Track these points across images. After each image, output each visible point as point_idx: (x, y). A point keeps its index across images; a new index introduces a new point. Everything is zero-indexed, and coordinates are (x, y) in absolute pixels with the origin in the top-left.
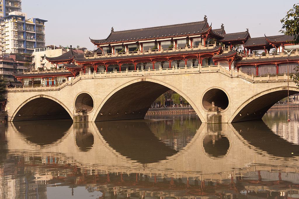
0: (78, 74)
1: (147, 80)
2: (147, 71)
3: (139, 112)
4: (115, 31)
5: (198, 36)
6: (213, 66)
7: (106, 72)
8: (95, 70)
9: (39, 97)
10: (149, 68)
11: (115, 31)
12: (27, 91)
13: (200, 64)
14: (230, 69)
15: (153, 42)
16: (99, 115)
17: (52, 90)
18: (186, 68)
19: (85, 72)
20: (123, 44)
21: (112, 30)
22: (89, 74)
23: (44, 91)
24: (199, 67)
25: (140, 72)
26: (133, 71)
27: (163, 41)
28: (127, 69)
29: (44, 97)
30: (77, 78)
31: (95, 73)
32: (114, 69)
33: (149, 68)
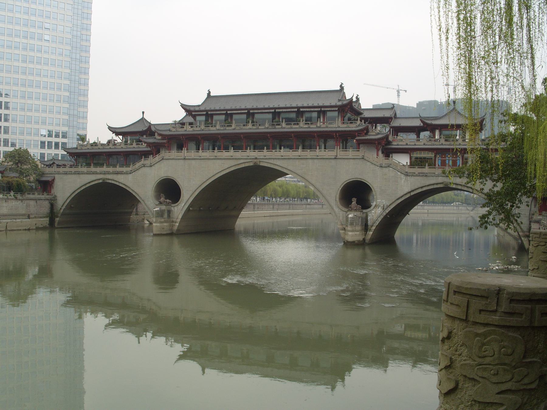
0: (158, 152)
1: (262, 164)
2: (263, 151)
3: (201, 209)
4: (212, 94)
5: (237, 112)
6: (342, 151)
7: (218, 150)
8: (184, 147)
9: (101, 181)
10: (265, 148)
11: (212, 94)
12: (83, 173)
13: (185, 148)
14: (378, 155)
15: (335, 111)
16: (188, 210)
17: (121, 173)
18: (265, 150)
19: (169, 148)
20: (275, 111)
21: (209, 94)
22: (174, 153)
23: (109, 173)
24: (183, 151)
25: (226, 152)
26: (258, 151)
27: (283, 112)
28: (300, 147)
29: (108, 181)
30: (158, 158)
31: (186, 151)
32: (230, 147)
33: (265, 148)
